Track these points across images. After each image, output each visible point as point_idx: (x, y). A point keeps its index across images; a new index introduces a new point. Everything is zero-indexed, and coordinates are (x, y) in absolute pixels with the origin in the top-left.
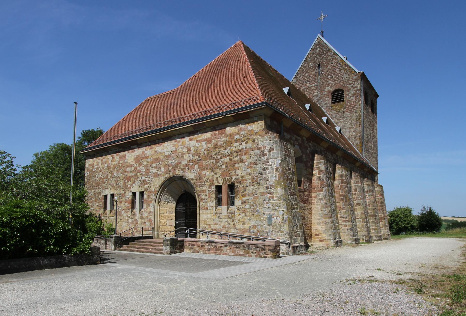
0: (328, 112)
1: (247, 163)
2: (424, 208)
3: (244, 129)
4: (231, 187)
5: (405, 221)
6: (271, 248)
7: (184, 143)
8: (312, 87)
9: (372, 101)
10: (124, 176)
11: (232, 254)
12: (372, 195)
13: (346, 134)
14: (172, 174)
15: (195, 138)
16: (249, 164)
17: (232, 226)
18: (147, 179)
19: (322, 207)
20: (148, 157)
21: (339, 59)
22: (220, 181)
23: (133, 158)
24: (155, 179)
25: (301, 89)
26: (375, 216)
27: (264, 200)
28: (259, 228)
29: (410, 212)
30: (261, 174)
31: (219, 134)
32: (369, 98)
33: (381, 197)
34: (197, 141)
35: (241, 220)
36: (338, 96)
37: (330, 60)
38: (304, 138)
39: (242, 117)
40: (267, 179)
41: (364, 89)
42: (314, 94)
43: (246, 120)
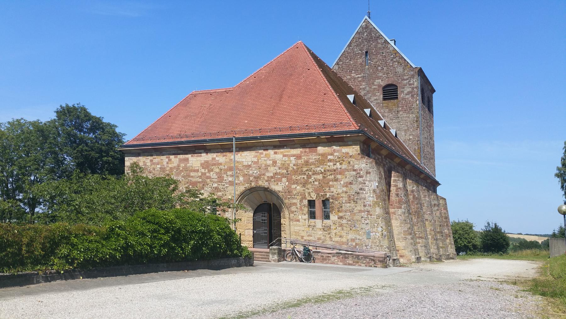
0: (378, 109)
1: (342, 182)
2: (489, 224)
3: (338, 151)
4: (325, 203)
5: (466, 238)
6: (381, 259)
7: (267, 156)
8: (358, 77)
9: (428, 97)
10: (187, 180)
11: (341, 263)
12: (438, 210)
13: (402, 137)
14: (253, 185)
15: (282, 153)
16: (344, 183)
17: (328, 239)
18: (220, 187)
19: (401, 223)
20: (221, 164)
21: (391, 49)
22: (313, 196)
23: (199, 162)
24: (231, 188)
25: (345, 79)
26: (442, 233)
27: (362, 217)
28: (357, 241)
29: (471, 228)
30: (358, 193)
31: (310, 152)
32: (426, 94)
33: (445, 211)
34: (284, 156)
35: (338, 234)
36: (390, 92)
37: (380, 48)
38: (383, 157)
39: (335, 139)
40: (365, 199)
41: (421, 86)
42: (361, 87)
43: (340, 143)
